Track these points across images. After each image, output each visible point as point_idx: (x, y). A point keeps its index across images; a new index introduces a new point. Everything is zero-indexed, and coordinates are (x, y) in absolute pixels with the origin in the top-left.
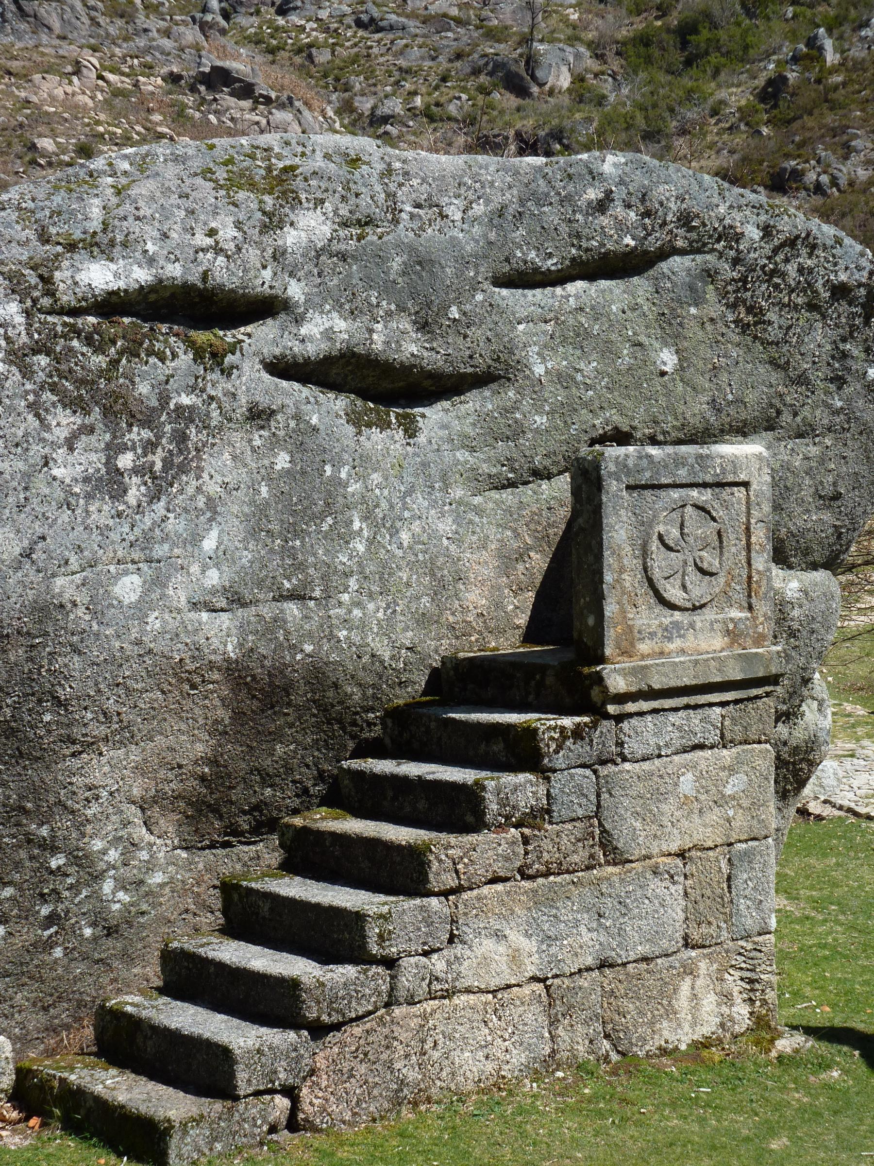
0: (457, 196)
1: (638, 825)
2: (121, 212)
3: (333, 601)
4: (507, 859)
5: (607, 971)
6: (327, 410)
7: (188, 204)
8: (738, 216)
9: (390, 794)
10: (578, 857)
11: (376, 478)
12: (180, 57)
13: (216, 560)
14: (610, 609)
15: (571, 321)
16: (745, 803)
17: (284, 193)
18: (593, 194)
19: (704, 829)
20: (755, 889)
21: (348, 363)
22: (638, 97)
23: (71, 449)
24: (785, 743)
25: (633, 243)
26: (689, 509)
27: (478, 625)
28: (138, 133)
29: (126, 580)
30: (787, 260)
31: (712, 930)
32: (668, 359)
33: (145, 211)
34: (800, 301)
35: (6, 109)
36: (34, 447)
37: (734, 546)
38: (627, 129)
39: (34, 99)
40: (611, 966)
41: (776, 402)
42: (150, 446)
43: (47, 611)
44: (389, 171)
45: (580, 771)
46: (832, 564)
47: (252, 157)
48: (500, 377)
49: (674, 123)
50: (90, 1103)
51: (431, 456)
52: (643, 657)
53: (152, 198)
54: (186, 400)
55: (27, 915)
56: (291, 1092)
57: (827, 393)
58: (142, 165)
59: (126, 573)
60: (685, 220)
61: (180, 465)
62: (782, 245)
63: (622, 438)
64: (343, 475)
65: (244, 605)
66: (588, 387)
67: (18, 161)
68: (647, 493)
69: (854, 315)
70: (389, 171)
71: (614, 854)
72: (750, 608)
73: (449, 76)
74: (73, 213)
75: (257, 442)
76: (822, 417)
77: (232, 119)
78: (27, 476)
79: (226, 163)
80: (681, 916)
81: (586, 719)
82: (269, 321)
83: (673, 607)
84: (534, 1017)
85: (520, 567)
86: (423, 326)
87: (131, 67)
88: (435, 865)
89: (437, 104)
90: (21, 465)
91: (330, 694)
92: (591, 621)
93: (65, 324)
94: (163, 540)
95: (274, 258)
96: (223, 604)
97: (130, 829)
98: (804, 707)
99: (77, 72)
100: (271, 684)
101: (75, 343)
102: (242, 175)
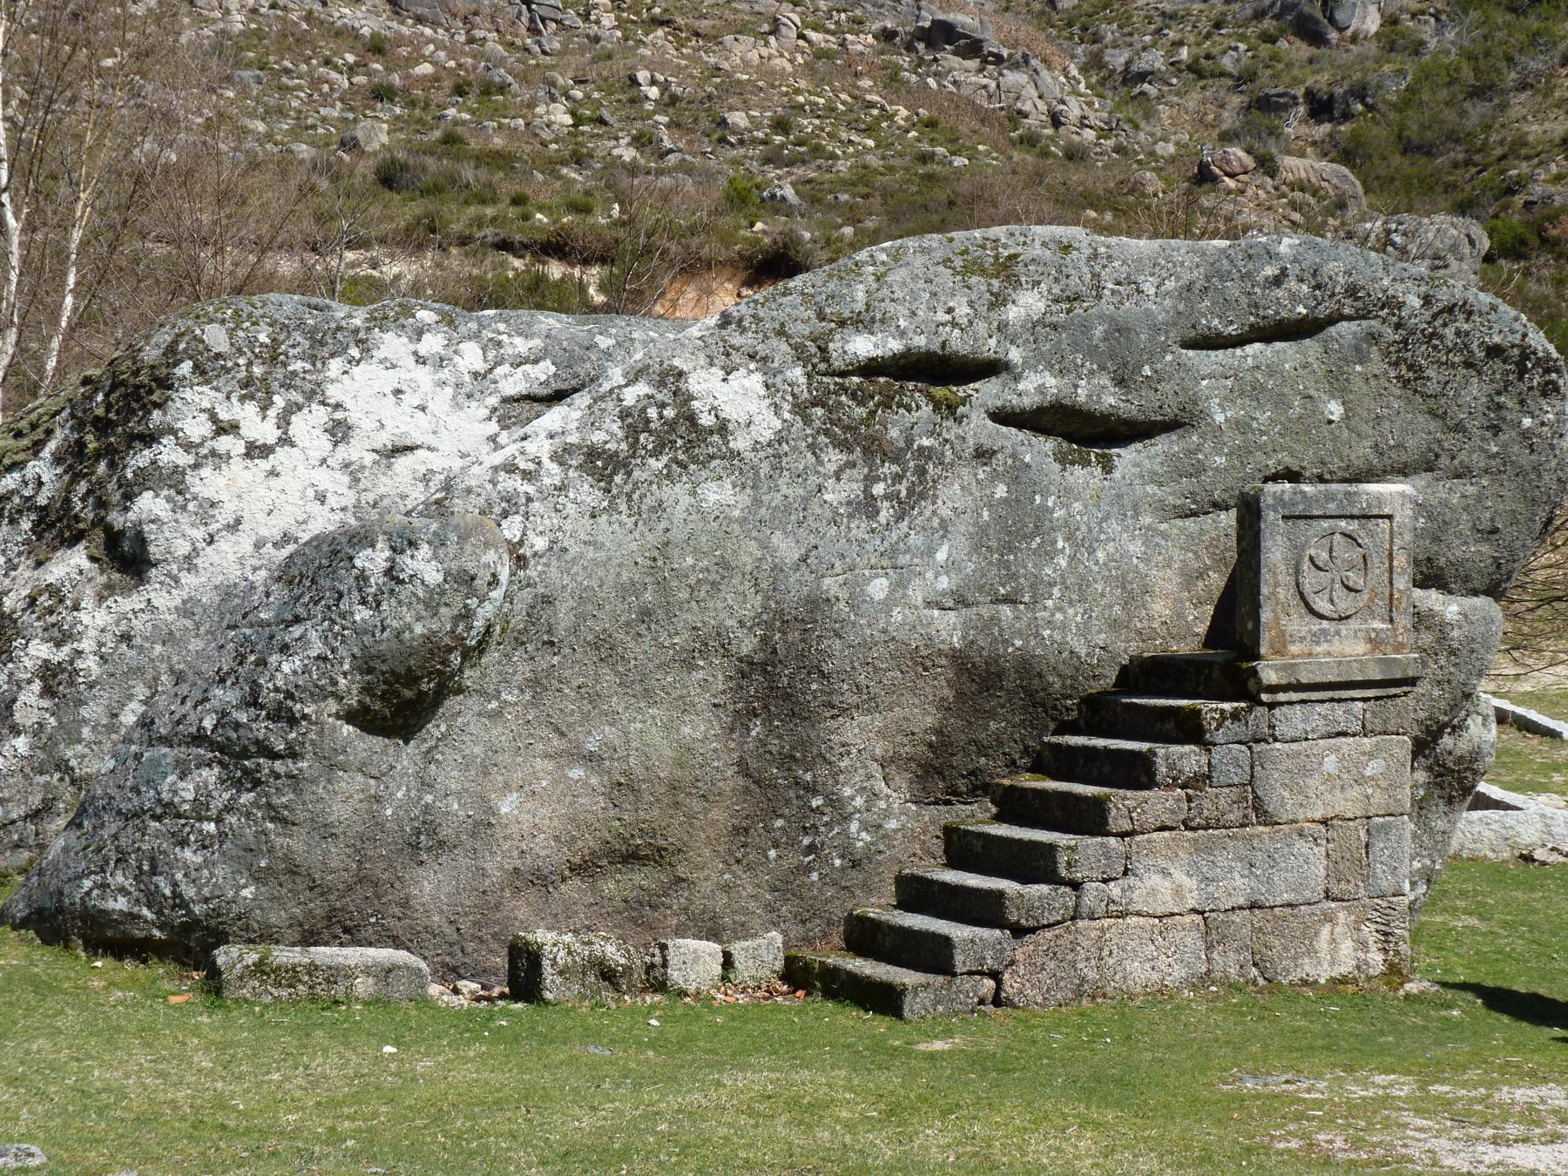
0: (1152, 275)
1: (1286, 794)
2: (880, 295)
3: (1039, 606)
4: (1173, 812)
5: (1257, 911)
6: (1039, 450)
7: (933, 288)
8: (1400, 287)
9: (1082, 761)
10: (1234, 816)
11: (1077, 506)
12: (895, 9)
13: (948, 568)
14: (1266, 615)
15: (1249, 378)
16: (1383, 784)
17: (1008, 277)
18: (1270, 271)
19: (1346, 803)
20: (1390, 856)
21: (1056, 412)
22: (1466, 43)
23: (838, 479)
24: (1450, 753)
25: (1304, 311)
26: (1337, 537)
27: (1163, 631)
28: (843, 103)
29: (877, 582)
30: (1445, 325)
31: (1351, 887)
32: (1335, 410)
33: (899, 294)
34: (1456, 359)
35: (694, 78)
36: (812, 478)
37: (1378, 569)
38: (1450, 84)
39: (725, 65)
40: (1260, 907)
41: (1435, 447)
42: (898, 478)
43: (817, 604)
44: (1095, 256)
45: (1236, 746)
46: (1494, 591)
47: (983, 247)
48: (1185, 424)
49: (1513, 75)
50: (844, 977)
51: (1124, 489)
52: (1294, 657)
53: (904, 283)
54: (926, 442)
55: (792, 843)
56: (995, 975)
57: (1483, 439)
58: (896, 256)
59: (877, 576)
60: (1352, 291)
61: (919, 494)
62: (1441, 312)
63: (1293, 476)
64: (1050, 504)
65: (967, 606)
66: (1262, 433)
67: (706, 140)
68: (1301, 522)
69: (1508, 372)
70: (1095, 256)
71: (1264, 816)
72: (1391, 621)
73: (1224, 21)
74: (843, 296)
75: (981, 476)
76: (1478, 461)
77: (955, 83)
78: (805, 499)
79: (962, 254)
80: (1323, 873)
81: (1243, 705)
82: (993, 379)
83: (1321, 617)
84: (1193, 941)
85: (1200, 584)
86: (1120, 382)
87: (837, 23)
88: (1114, 812)
89: (1208, 57)
90: (801, 491)
91: (1036, 682)
92: (1250, 626)
93: (836, 384)
94: (906, 552)
95: (999, 329)
96: (951, 604)
97: (872, 781)
98: (1469, 721)
99: (774, 31)
100: (987, 671)
101: (843, 398)
102: (974, 263)
